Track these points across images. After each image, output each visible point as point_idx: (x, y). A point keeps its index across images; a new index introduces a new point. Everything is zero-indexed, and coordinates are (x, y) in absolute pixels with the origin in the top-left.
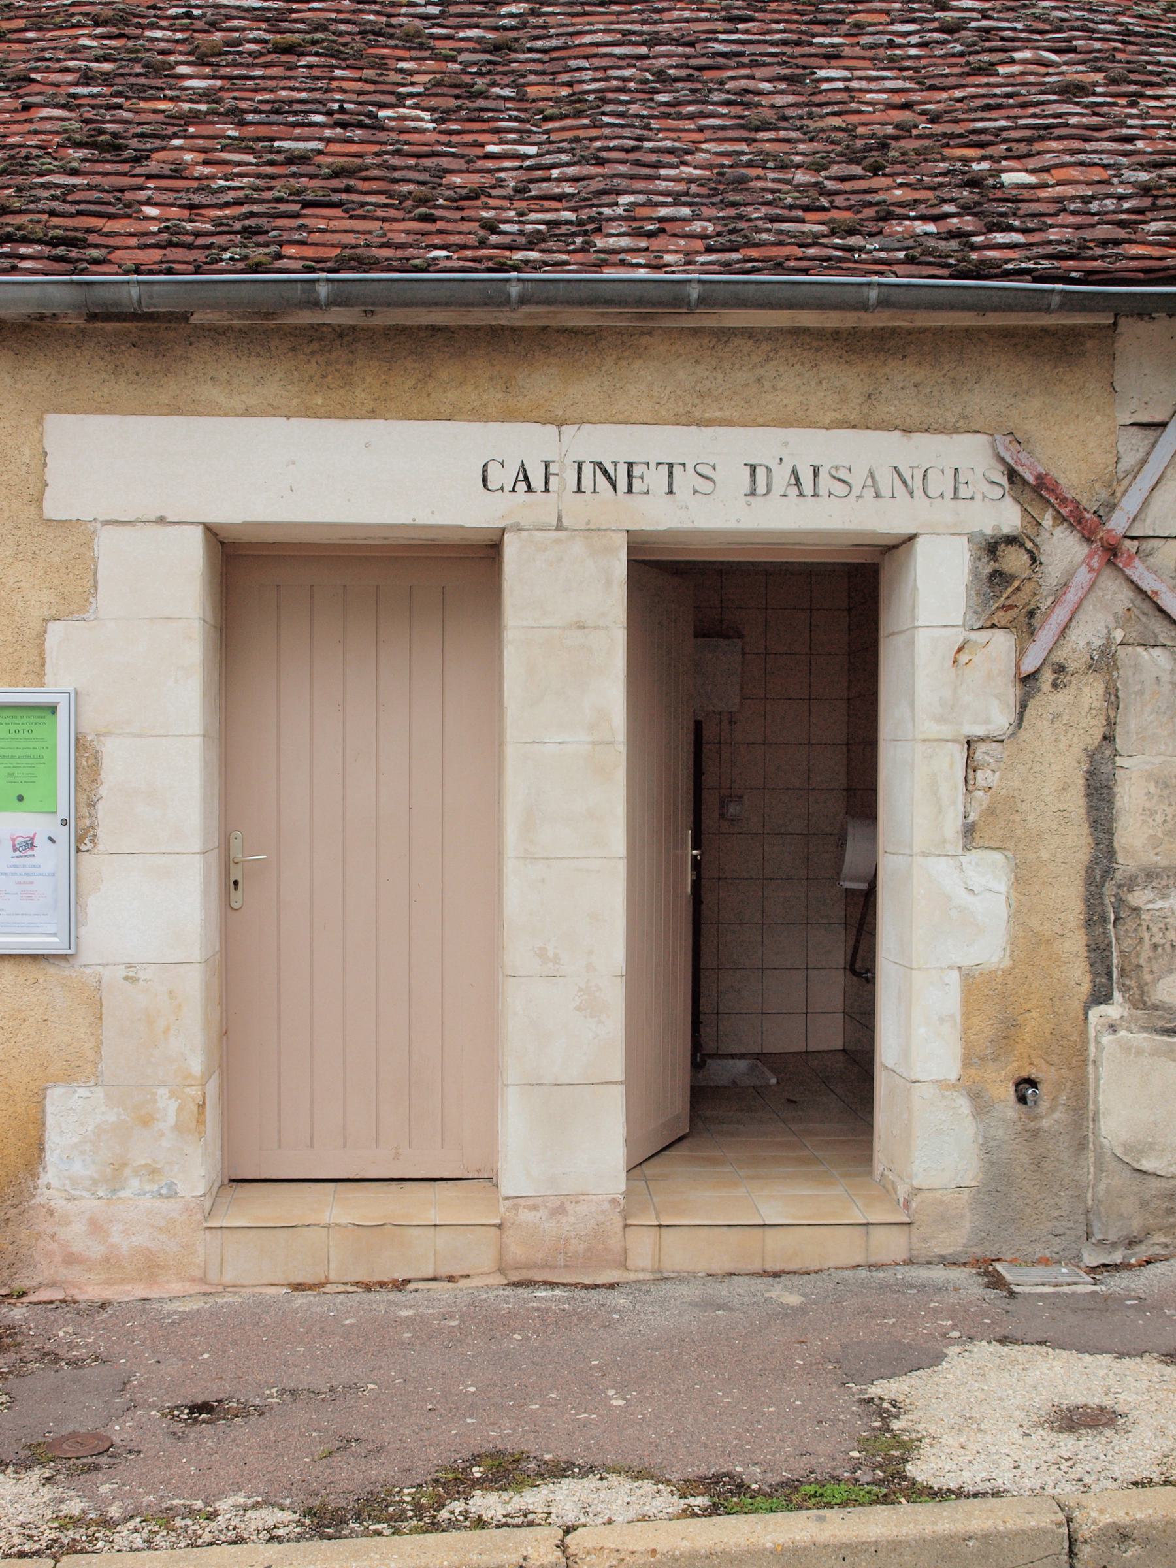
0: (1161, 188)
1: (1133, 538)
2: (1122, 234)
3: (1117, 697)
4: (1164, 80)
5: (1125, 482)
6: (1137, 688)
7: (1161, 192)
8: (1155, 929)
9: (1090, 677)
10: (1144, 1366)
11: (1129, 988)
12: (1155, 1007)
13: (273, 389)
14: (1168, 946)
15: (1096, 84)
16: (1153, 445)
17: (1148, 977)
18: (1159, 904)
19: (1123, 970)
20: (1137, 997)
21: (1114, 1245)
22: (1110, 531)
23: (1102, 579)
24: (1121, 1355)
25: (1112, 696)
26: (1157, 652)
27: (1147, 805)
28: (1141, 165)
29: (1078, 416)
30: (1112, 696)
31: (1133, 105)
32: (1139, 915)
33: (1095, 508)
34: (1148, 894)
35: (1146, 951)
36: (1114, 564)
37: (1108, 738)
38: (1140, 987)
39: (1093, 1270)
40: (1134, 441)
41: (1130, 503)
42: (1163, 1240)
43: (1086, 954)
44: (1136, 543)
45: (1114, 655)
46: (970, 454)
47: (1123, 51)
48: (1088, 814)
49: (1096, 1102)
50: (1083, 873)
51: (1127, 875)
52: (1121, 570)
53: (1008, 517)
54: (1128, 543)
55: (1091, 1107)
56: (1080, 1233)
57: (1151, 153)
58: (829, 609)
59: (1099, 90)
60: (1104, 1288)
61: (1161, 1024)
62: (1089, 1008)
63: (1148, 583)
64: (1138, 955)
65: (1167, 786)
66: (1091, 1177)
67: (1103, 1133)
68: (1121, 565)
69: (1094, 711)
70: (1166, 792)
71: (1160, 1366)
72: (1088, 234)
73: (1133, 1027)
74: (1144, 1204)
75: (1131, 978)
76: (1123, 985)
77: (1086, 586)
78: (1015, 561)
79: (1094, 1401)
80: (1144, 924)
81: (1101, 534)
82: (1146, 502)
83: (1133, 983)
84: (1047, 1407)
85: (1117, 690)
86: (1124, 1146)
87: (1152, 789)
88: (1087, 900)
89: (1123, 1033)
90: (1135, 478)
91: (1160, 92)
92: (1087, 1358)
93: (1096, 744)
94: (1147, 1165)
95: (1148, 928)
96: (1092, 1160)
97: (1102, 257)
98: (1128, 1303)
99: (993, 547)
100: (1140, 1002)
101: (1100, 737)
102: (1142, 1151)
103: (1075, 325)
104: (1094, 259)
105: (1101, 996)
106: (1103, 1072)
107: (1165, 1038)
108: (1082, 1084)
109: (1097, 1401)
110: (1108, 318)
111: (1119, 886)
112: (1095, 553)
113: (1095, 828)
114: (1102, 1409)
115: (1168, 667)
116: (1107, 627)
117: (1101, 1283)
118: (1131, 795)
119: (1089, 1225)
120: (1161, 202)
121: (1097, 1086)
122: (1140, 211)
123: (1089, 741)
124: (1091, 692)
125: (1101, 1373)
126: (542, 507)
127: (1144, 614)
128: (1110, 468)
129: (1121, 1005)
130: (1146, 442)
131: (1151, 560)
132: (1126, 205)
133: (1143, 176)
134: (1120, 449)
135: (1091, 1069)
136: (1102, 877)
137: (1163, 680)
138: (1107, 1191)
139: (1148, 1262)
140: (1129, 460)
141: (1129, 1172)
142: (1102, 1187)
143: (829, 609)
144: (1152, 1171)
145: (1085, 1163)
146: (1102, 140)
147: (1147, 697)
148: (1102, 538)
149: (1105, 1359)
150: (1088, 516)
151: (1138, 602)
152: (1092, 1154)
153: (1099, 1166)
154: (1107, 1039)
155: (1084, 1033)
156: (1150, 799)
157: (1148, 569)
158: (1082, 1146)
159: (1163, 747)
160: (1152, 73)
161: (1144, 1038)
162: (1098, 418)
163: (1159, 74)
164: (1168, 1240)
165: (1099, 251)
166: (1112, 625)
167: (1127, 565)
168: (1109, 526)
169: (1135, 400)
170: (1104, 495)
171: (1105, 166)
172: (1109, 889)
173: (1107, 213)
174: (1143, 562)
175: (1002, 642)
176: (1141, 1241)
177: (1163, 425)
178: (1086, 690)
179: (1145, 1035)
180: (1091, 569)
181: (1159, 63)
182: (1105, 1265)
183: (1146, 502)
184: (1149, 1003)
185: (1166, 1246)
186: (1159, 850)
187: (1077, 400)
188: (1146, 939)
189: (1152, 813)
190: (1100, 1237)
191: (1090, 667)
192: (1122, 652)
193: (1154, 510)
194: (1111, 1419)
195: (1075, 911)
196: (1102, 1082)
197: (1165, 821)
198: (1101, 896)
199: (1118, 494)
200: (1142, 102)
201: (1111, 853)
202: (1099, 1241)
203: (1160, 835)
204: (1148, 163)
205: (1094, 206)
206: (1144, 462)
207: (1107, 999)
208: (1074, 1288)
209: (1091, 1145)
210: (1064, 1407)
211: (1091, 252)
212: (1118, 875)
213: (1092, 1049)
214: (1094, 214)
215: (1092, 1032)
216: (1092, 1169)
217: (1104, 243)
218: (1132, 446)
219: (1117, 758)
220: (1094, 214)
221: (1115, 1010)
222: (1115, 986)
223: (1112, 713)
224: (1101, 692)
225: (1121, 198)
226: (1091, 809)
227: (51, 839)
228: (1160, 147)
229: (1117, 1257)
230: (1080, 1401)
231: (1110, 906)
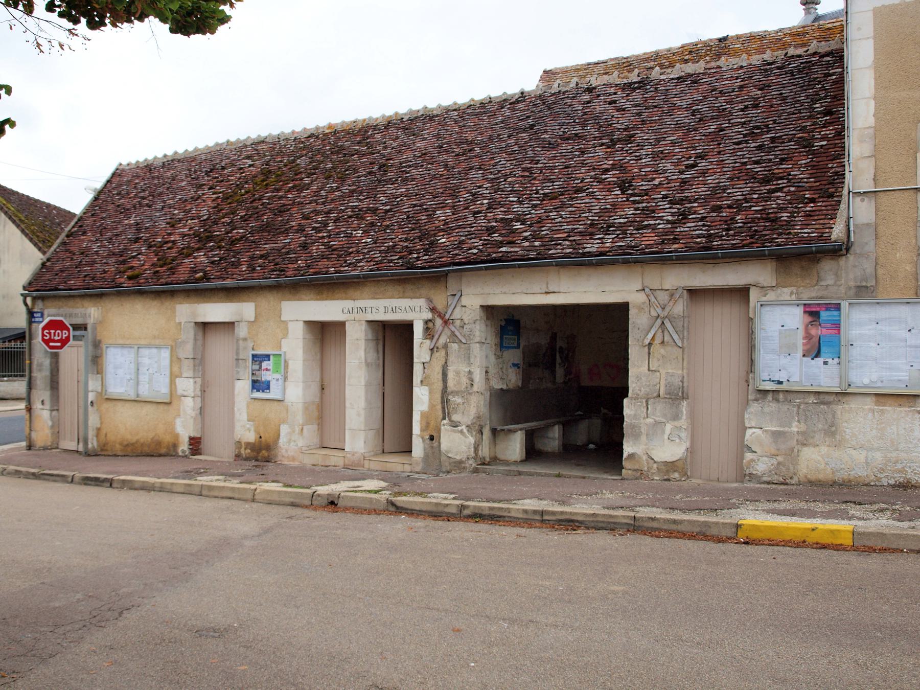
13: (312, 296)
25: (447, 354)
30: (447, 354)
37: (446, 363)
46: (421, 302)
53: (429, 316)
58: (406, 328)
78: (430, 325)
99: (426, 322)
100: (450, 420)
105: (444, 418)
118: (451, 375)
124: (443, 353)
126: (351, 317)
143: (406, 328)
175: (428, 341)
195: (439, 400)
221: (445, 422)
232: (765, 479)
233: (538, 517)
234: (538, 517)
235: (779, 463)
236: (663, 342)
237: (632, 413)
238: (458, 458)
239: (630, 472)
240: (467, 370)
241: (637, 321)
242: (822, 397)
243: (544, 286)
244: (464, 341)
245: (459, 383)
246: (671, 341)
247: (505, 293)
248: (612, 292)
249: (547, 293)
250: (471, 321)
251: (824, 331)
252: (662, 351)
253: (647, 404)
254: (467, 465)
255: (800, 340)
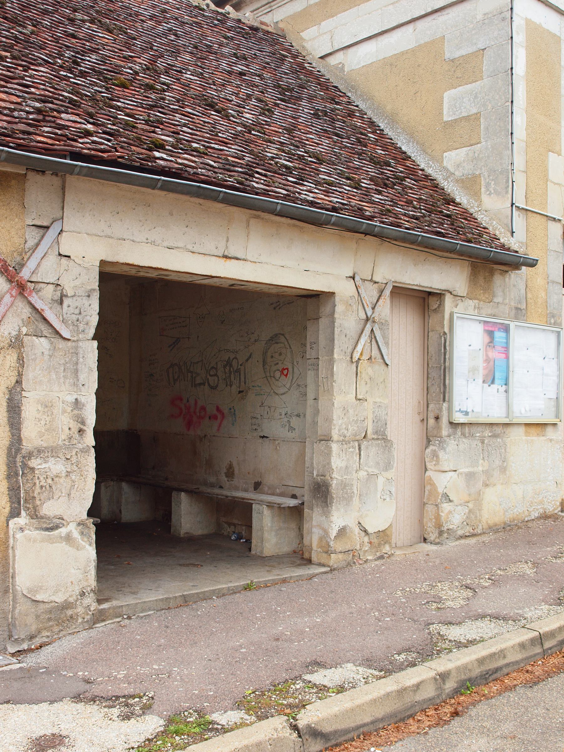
0: (46, 112)
1: (31, 282)
2: (31, 130)
3: (23, 361)
4: (38, 63)
5: (29, 254)
6: (33, 357)
7: (47, 114)
8: (42, 478)
9: (10, 351)
10: (66, 706)
11: (28, 508)
12: (42, 518)
14: (48, 486)
15: (7, 57)
16: (43, 237)
17: (38, 503)
18: (44, 466)
19: (26, 499)
20: (33, 513)
21: (23, 640)
22: (21, 277)
23: (16, 301)
24: (52, 702)
25: (21, 360)
26: (42, 339)
27: (38, 416)
28: (36, 99)
29: (6, 218)
30: (21, 360)
31: (26, 71)
32: (34, 472)
33: (13, 265)
34: (39, 461)
35: (37, 490)
36: (23, 294)
37: (19, 382)
38: (35, 508)
39: (13, 655)
40: (33, 234)
41: (31, 264)
42: (47, 634)
43: (7, 493)
44: (33, 284)
45: (22, 340)
47: (16, 46)
48: (8, 420)
49: (14, 568)
50: (6, 451)
51: (28, 451)
52: (26, 297)
54: (29, 284)
55: (11, 571)
56: (6, 636)
57: (38, 95)
59: (8, 60)
60: (25, 665)
61: (45, 526)
62: (9, 520)
63: (39, 305)
64: (33, 492)
65: (46, 407)
66: (10, 607)
67: (18, 583)
68: (26, 295)
69: (12, 368)
70: (46, 410)
71: (74, 704)
72: (15, 126)
73: (31, 528)
74: (37, 617)
75: (30, 504)
76: (26, 507)
77: (9, 304)
79: (49, 732)
80: (36, 476)
81: (17, 278)
82: (39, 265)
83: (31, 506)
84: (25, 741)
85: (23, 358)
86: (28, 589)
87: (40, 408)
88: (8, 465)
89: (27, 532)
90: (34, 252)
91: (37, 68)
92: (35, 707)
93: (13, 385)
94: (39, 597)
95: (38, 478)
96: (11, 598)
97: (24, 139)
98: (41, 671)
100: (34, 515)
101: (15, 381)
102: (37, 591)
103: (7, 172)
104: (20, 139)
105: (15, 513)
106: (18, 553)
107: (47, 533)
108: (6, 560)
109: (50, 731)
110: (23, 170)
111: (24, 457)
112: (14, 288)
113: (12, 427)
114: (53, 735)
115: (48, 347)
116: (19, 326)
117: (23, 662)
118: (30, 410)
119: (10, 631)
120: (47, 118)
121: (14, 560)
122: (38, 121)
123: (9, 383)
125: (46, 714)
127: (37, 320)
128: (22, 246)
129: (25, 517)
130: (39, 235)
131: (40, 293)
132: (31, 117)
133: (38, 105)
134: (26, 237)
135: (10, 551)
136: (15, 452)
137: (45, 353)
138: (20, 613)
139: (41, 647)
140: (31, 243)
141: (30, 602)
142: (17, 611)
144: (41, 600)
145: (7, 600)
146: (14, 83)
147: (37, 361)
148: (17, 281)
149: (44, 706)
150: (11, 269)
151: (34, 314)
152: (11, 595)
153: (14, 600)
154: (19, 535)
155: (7, 533)
156: (38, 413)
157: (39, 298)
158: (6, 591)
159: (45, 387)
160: (31, 59)
161: (37, 534)
162: (17, 220)
163: (35, 60)
164: (49, 634)
165: (21, 136)
166: (21, 325)
167: (29, 295)
168: (21, 274)
169: (34, 213)
170: (18, 259)
171: (18, 96)
172: (19, 459)
173: (22, 118)
174: (37, 294)
176: (36, 636)
177: (47, 228)
178: (8, 357)
179: (38, 532)
180: (12, 296)
181: (34, 55)
182: (19, 651)
183: (39, 265)
184: (39, 516)
185: (48, 637)
186: (42, 439)
187: (6, 210)
188: (37, 483)
189: (40, 420)
190: (16, 637)
191: (10, 345)
192: (26, 339)
193: (41, 269)
194: (60, 740)
196: (16, 558)
197: (46, 424)
198: (15, 462)
199: (25, 259)
200: (30, 71)
201: (20, 440)
202: (16, 639)
203: (43, 431)
204: (38, 99)
205: (16, 114)
206: (38, 245)
207: (18, 515)
208: (10, 667)
209: (11, 591)
210: (34, 738)
211: (18, 136)
212: (23, 452)
213: (11, 541)
214: (16, 118)
215: (11, 533)
216: (11, 603)
217: (24, 132)
218: (32, 236)
219: (23, 392)
220: (16, 118)
221: (23, 520)
222: (22, 508)
223: (20, 369)
224: (15, 358)
225: (28, 113)
226: (9, 418)
227: (544, 358)
228: (42, 93)
229: (25, 646)
230: (42, 733)
231: (19, 467)
232: (460, 532)
233: (538, 650)
234: (538, 650)
235: (470, 511)
236: (370, 359)
237: (343, 464)
238: (60, 598)
239: (340, 556)
240: (71, 399)
241: (346, 319)
242: (495, 428)
243: (222, 244)
244: (65, 333)
245: (51, 429)
246: (379, 356)
247: (153, 243)
248: (317, 273)
249: (226, 257)
250: (81, 292)
251: (497, 354)
252: (370, 370)
253: (360, 449)
254: (80, 610)
255: (480, 364)
